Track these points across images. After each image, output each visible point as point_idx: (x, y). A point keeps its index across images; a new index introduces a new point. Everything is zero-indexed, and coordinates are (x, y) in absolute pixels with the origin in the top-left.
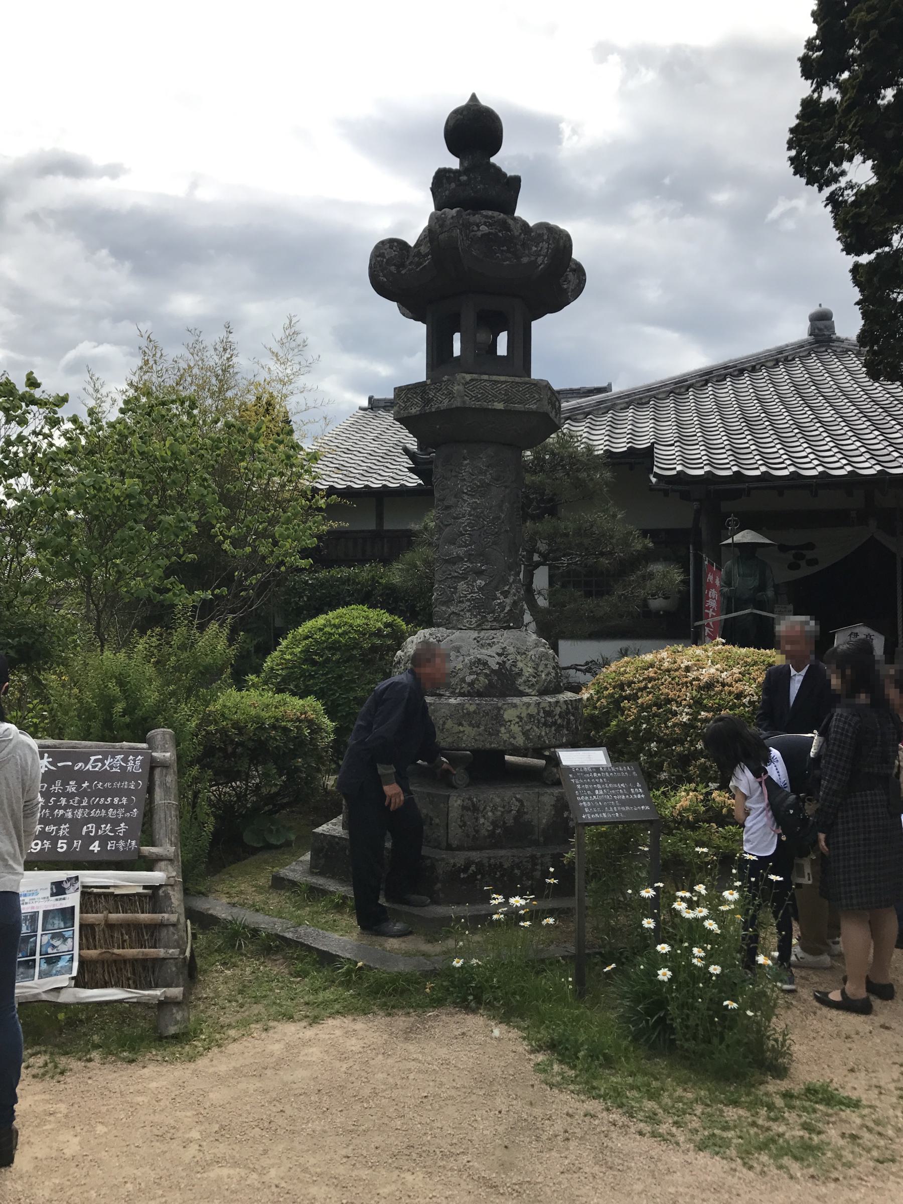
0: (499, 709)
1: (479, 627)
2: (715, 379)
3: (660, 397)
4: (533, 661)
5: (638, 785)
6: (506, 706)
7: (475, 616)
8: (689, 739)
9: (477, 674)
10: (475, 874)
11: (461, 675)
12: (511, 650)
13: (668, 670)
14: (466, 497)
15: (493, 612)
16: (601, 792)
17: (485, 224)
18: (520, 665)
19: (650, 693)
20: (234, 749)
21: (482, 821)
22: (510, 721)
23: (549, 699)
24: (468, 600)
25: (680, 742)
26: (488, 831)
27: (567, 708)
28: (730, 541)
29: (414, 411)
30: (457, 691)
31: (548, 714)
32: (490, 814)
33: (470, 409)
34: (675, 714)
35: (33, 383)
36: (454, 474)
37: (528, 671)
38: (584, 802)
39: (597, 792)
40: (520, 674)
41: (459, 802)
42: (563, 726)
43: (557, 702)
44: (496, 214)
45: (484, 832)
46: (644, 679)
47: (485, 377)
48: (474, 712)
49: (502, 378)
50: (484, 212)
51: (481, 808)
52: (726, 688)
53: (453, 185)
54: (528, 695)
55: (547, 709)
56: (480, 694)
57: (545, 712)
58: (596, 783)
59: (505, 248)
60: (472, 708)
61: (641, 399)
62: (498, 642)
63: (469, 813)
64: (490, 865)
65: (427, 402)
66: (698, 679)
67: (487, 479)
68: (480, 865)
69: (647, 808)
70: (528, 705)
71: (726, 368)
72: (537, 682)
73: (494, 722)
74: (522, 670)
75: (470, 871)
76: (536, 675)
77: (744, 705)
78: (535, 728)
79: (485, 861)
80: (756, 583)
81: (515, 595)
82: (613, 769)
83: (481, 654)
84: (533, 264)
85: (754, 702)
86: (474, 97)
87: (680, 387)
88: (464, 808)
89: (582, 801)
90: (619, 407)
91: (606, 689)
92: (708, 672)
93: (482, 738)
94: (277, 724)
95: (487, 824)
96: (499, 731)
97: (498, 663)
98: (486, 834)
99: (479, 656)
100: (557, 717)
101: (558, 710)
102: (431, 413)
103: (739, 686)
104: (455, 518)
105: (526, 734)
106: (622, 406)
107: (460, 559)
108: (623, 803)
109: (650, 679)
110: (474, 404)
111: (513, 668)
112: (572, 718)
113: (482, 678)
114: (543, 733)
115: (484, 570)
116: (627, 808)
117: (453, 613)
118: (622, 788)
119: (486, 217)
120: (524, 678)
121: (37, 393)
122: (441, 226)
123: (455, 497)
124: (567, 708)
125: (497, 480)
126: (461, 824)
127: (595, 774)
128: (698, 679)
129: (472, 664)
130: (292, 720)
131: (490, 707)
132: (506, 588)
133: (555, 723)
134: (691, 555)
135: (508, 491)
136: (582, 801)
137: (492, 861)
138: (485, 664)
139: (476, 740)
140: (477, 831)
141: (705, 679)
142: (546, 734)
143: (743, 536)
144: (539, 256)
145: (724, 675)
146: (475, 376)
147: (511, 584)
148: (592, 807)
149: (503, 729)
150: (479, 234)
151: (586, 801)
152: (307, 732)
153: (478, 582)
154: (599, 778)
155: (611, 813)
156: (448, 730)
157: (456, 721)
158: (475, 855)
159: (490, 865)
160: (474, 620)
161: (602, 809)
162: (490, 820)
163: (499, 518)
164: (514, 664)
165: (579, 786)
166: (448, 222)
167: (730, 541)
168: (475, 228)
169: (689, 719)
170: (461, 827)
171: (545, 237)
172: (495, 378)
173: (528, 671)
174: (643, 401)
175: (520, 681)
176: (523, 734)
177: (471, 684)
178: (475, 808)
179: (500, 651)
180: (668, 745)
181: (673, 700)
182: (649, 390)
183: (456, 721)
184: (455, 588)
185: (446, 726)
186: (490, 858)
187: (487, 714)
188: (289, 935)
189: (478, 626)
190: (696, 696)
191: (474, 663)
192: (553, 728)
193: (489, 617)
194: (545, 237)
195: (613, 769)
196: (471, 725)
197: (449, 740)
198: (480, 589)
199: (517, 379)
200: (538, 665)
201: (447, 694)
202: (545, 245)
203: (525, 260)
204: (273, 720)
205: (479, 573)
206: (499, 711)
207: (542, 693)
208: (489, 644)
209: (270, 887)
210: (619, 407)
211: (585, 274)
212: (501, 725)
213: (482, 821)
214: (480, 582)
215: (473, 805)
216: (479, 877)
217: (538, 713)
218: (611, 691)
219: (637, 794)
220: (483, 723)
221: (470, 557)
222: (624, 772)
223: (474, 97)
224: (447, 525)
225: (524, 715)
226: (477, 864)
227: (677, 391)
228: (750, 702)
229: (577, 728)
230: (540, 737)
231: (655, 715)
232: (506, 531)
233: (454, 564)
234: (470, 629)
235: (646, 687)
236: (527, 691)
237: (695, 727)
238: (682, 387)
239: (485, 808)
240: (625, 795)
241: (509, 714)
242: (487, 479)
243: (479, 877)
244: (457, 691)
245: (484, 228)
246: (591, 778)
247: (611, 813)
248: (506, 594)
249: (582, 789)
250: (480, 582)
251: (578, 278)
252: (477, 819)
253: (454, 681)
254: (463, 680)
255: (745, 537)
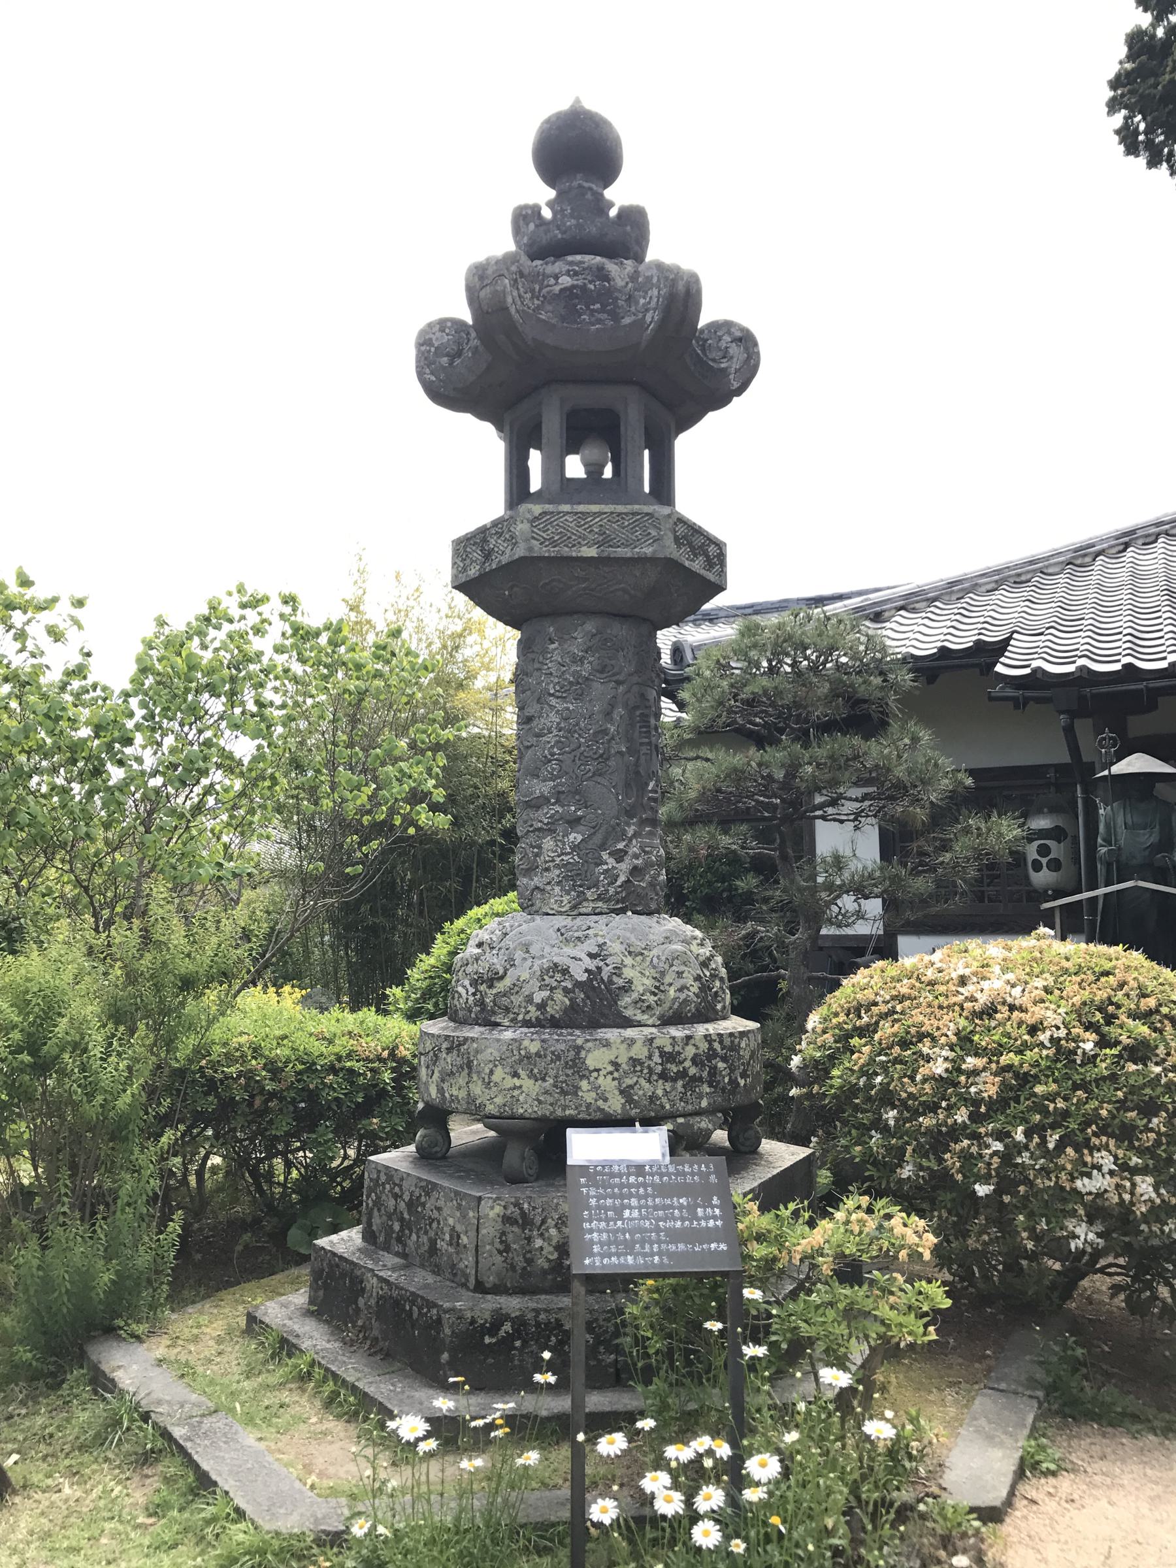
0: (578, 1049)
1: (575, 910)
2: (1140, 542)
3: (1050, 571)
4: (654, 967)
5: (715, 1201)
6: (590, 1044)
7: (568, 893)
8: (944, 1104)
9: (552, 989)
10: (510, 1338)
11: (526, 991)
12: (616, 947)
13: (932, 983)
14: (553, 701)
15: (596, 885)
16: (636, 1214)
17: (568, 273)
18: (628, 973)
19: (895, 1021)
20: (266, 1101)
21: (539, 1243)
22: (598, 1070)
23: (677, 1032)
24: (557, 867)
25: (933, 1108)
26: (549, 1261)
27: (711, 1048)
28: (1106, 773)
29: (473, 572)
30: (520, 1017)
31: (669, 1057)
32: (553, 1231)
33: (541, 559)
34: (928, 1059)
35: (25, 582)
36: (537, 665)
37: (642, 983)
38: (595, 1232)
39: (627, 1213)
40: (627, 988)
41: (498, 1209)
42: (700, 1079)
43: (689, 1038)
44: (587, 258)
45: (541, 1262)
46: (893, 998)
47: (566, 508)
48: (538, 1054)
49: (595, 508)
50: (570, 258)
51: (538, 1220)
52: (1016, 1013)
53: (532, 226)
54: (640, 1024)
55: (668, 1049)
56: (555, 1023)
57: (662, 1054)
58: (630, 1196)
59: (598, 306)
60: (534, 1047)
61: (1019, 575)
62: (596, 935)
63: (515, 1229)
64: (538, 1325)
65: (488, 556)
66: (973, 999)
67: (586, 670)
68: (520, 1323)
69: (723, 1247)
70: (631, 1042)
71: (1158, 524)
72: (659, 1003)
73: (570, 1072)
74: (630, 982)
75: (502, 1333)
76: (658, 990)
77: (1042, 1045)
78: (643, 1082)
79: (530, 1316)
80: (1154, 838)
81: (636, 856)
82: (672, 1169)
83: (559, 955)
84: (640, 324)
85: (1060, 1039)
86: (578, 101)
87: (1085, 555)
88: (507, 1219)
89: (591, 1231)
90: (984, 589)
91: (836, 1015)
92: (994, 986)
93: (550, 1099)
94: (338, 1066)
95: (548, 1249)
96: (578, 1088)
97: (587, 970)
98: (546, 1266)
99: (556, 959)
100: (687, 1064)
101: (690, 1051)
102: (492, 571)
103: (1036, 1013)
104: (538, 735)
105: (625, 1092)
106: (989, 587)
107: (543, 801)
108: (675, 1236)
109: (901, 998)
110: (546, 551)
111: (615, 979)
112: (721, 1065)
113: (559, 995)
114: (660, 1092)
115: (580, 818)
116: (681, 1246)
117: (537, 888)
118: (681, 1207)
119: (571, 263)
120: (635, 995)
121: (29, 593)
122: (481, 278)
123: (539, 701)
124: (711, 1048)
125: (602, 672)
126: (501, 1247)
127: (632, 1179)
128: (973, 999)
129: (544, 972)
130: (367, 1059)
131: (563, 1047)
132: (621, 846)
133: (683, 1074)
134: (1080, 801)
135: (621, 689)
136: (591, 1231)
137: (542, 1316)
138: (565, 972)
139: (540, 1102)
140: (530, 1262)
141: (983, 999)
142: (666, 1093)
143: (1128, 764)
144: (647, 310)
145: (1016, 992)
146: (549, 507)
147: (630, 840)
148: (609, 1243)
149: (584, 1084)
150: (557, 289)
151: (600, 1231)
152: (387, 1076)
153: (571, 837)
154: (638, 1186)
155: (645, 1255)
156: (496, 1084)
157: (508, 1070)
158: (513, 1304)
159: (538, 1325)
160: (566, 899)
161: (629, 1247)
162: (554, 1242)
163: (605, 732)
164: (618, 970)
165: (593, 1202)
166: (490, 272)
167: (1106, 773)
168: (552, 281)
169: (947, 1070)
170: (500, 1252)
171: (655, 280)
172: (581, 508)
173: (642, 983)
174: (1023, 578)
175: (626, 1000)
176: (622, 1092)
177: (542, 1006)
178: (525, 1221)
179: (595, 950)
180: (916, 1114)
181: (929, 1035)
182: (1031, 562)
183: (508, 1070)
184: (540, 847)
185: (494, 1078)
186: (537, 1311)
187: (559, 1058)
188: (178, 1432)
189: (574, 907)
190: (964, 1028)
191: (548, 971)
192: (680, 1083)
193: (589, 894)
194: (655, 280)
195: (672, 1169)
196: (531, 1075)
197: (499, 1100)
198: (575, 848)
199: (620, 508)
200: (663, 974)
201: (506, 1022)
202: (655, 292)
203: (627, 321)
204: (333, 1057)
205: (574, 822)
206: (578, 1053)
207: (676, 1018)
208: (578, 938)
209: (243, 1332)
210: (984, 589)
211: (756, 344)
212: (582, 1077)
213: (539, 1243)
214: (575, 837)
215: (523, 1214)
216: (518, 1344)
217: (650, 1057)
218: (842, 1018)
219: (707, 1218)
220: (552, 1073)
221: (559, 797)
222: (693, 1174)
223: (578, 101)
224: (528, 747)
225: (623, 1060)
226: (513, 1320)
227: (1078, 562)
228: (1052, 1039)
229: (733, 1082)
230: (653, 1098)
231: (898, 1060)
232: (620, 753)
233: (538, 808)
234: (561, 913)
235: (893, 1012)
236: (640, 1017)
237: (956, 1084)
238: (1085, 555)
239: (544, 1222)
240: (683, 1219)
241: (596, 1058)
242: (586, 670)
243: (518, 1344)
244: (520, 1017)
245: (565, 281)
246: (621, 1186)
247: (645, 1255)
248: (619, 856)
249: (599, 1207)
250: (575, 837)
251: (746, 349)
252: (529, 1239)
253: (517, 1000)
254: (529, 999)
255: (1137, 763)
